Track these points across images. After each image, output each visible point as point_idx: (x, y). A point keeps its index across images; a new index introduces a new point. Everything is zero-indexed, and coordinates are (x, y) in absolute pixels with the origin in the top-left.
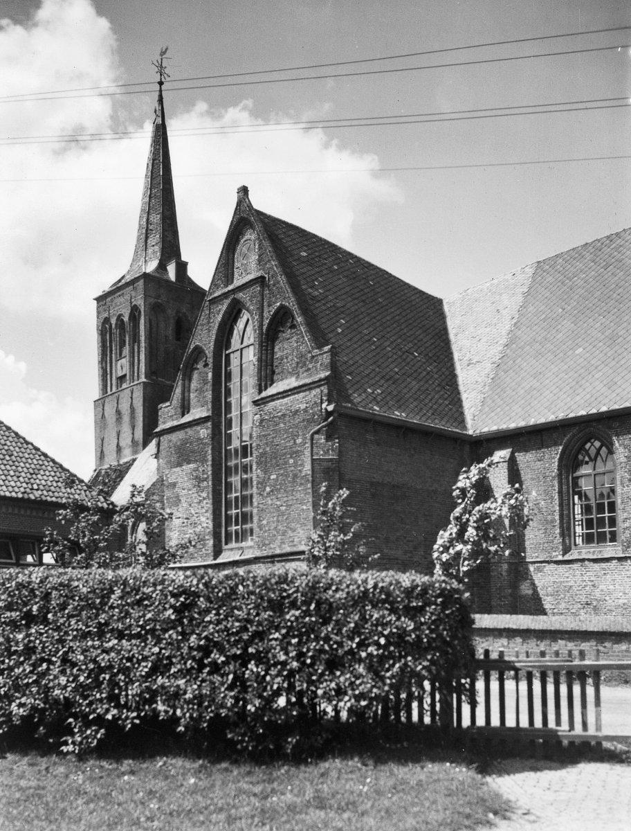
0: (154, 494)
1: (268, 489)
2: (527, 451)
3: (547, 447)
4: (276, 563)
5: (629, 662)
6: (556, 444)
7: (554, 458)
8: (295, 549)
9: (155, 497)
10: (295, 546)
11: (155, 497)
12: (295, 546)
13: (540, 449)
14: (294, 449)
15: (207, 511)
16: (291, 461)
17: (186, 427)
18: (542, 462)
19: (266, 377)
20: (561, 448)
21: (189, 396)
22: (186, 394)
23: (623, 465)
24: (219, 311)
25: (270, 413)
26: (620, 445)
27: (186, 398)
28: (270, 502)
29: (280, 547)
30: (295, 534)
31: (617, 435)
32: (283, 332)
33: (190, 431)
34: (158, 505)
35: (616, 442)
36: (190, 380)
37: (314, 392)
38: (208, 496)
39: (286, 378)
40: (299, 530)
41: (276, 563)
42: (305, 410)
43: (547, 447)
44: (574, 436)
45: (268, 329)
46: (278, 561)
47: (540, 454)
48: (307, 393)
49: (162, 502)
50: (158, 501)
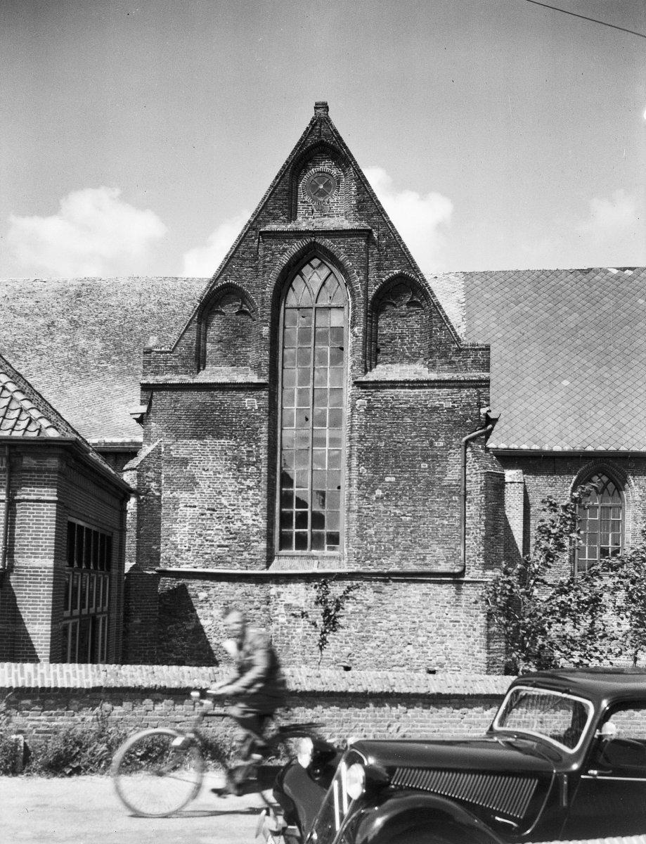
0: (148, 469)
1: (379, 493)
2: (536, 474)
3: (560, 475)
4: (391, 582)
5: (642, 685)
6: (570, 473)
7: (567, 486)
8: (426, 569)
9: (150, 474)
10: (426, 565)
11: (150, 474)
12: (426, 565)
13: (552, 475)
14: (431, 453)
15: (255, 505)
16: (424, 465)
17: (215, 390)
18: (553, 488)
19: (370, 355)
20: (575, 477)
21: (205, 346)
22: (202, 343)
23: (638, 503)
24: (285, 250)
25: (387, 402)
26: (636, 485)
27: (202, 348)
28: (382, 508)
29: (399, 563)
30: (427, 551)
31: (633, 475)
32: (394, 305)
33: (220, 396)
34: (153, 484)
35: (632, 481)
36: (207, 325)
37: (465, 392)
38: (258, 486)
39: (401, 362)
40: (435, 547)
41: (391, 582)
42: (451, 410)
43: (560, 475)
44: (588, 467)
45: (375, 297)
46: (395, 581)
47: (551, 479)
48: (455, 390)
49: (159, 482)
50: (153, 480)
